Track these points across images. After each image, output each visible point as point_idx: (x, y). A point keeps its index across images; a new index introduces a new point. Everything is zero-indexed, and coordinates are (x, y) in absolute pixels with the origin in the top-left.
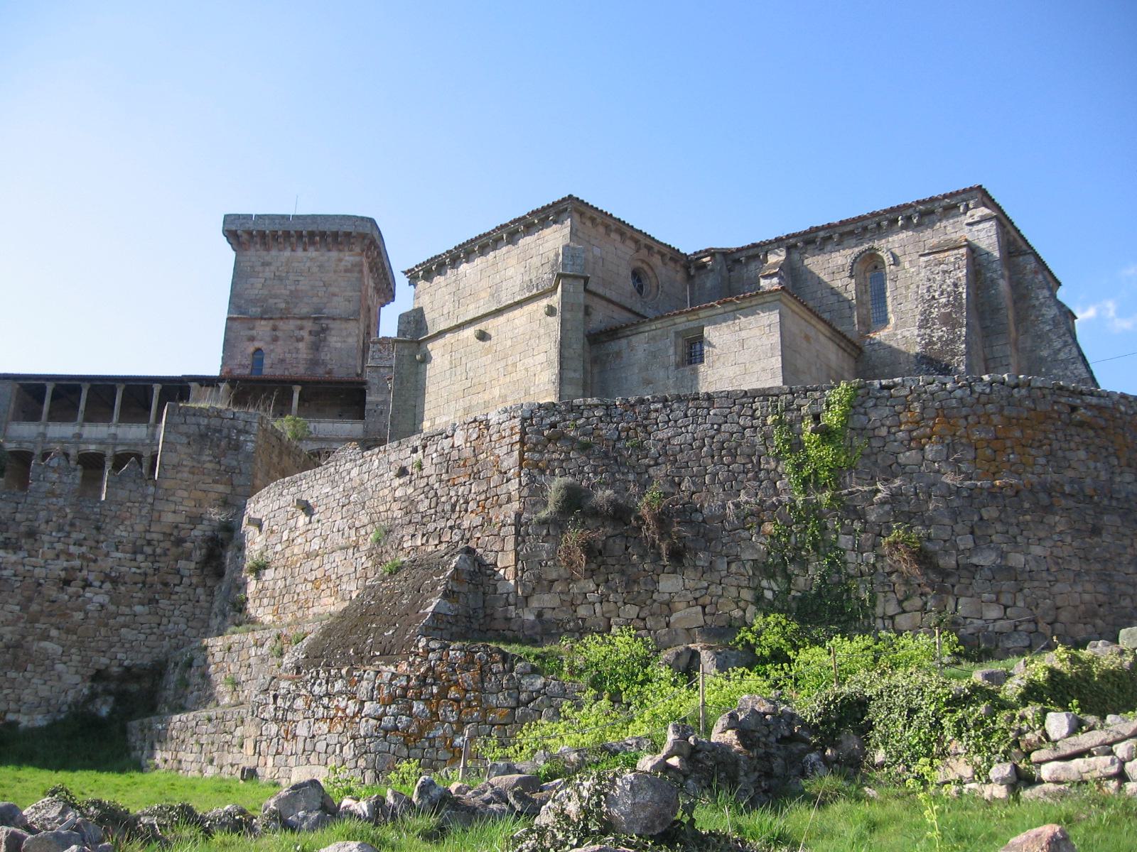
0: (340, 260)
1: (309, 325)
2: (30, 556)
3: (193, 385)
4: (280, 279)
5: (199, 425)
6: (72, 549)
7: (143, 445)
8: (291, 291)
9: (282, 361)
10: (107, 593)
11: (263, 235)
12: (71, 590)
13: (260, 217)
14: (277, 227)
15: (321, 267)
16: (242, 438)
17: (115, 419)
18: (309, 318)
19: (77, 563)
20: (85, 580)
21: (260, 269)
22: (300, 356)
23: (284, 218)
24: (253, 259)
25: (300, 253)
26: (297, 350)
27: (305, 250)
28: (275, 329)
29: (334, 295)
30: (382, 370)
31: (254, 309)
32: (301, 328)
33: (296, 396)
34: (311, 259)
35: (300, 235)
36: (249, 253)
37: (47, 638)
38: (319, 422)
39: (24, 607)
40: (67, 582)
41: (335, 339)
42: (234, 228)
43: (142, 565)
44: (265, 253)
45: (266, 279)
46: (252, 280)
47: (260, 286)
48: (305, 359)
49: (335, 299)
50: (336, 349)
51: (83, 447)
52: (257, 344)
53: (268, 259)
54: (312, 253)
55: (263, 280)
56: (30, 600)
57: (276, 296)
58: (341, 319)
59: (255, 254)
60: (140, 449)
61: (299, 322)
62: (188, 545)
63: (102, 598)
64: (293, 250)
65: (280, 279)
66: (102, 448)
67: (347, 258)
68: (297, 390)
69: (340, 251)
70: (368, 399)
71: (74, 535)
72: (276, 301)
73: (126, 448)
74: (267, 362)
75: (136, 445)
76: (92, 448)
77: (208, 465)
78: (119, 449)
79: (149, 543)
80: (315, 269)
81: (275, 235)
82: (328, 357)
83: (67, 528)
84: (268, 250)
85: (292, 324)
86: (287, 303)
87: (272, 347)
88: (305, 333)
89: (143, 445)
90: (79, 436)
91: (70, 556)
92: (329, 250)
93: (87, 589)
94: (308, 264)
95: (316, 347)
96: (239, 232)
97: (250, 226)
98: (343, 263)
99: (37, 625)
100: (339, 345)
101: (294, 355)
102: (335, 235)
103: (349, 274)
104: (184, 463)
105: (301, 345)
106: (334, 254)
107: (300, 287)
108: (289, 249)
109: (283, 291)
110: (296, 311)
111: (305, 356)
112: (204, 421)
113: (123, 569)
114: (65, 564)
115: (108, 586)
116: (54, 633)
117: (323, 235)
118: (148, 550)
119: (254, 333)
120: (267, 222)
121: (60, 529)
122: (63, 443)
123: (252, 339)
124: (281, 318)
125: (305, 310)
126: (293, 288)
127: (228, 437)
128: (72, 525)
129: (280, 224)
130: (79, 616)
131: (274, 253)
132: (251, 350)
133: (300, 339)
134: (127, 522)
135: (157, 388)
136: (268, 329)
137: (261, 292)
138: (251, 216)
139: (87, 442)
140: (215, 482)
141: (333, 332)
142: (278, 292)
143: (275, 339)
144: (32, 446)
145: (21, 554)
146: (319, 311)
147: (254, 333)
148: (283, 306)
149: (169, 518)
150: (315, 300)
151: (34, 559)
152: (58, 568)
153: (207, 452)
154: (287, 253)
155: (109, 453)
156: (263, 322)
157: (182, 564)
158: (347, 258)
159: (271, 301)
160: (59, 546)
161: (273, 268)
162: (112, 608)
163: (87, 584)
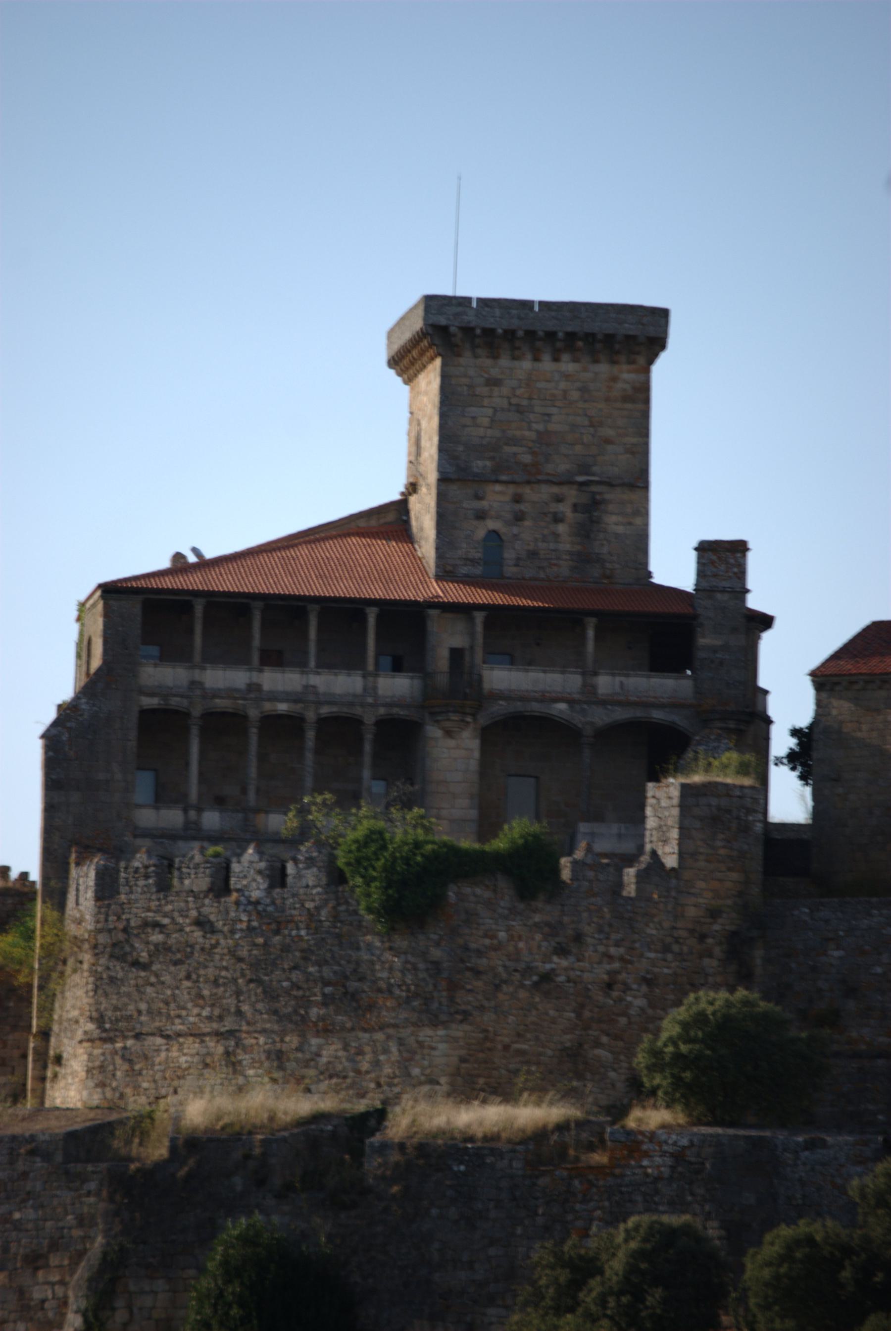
0: (614, 379)
1: (572, 494)
2: (579, 960)
3: (433, 612)
4: (519, 410)
5: (710, 805)
6: (613, 950)
7: (363, 705)
8: (538, 432)
9: (533, 554)
10: (645, 996)
11: (489, 333)
12: (615, 994)
13: (486, 303)
14: (515, 323)
15: (584, 390)
16: (751, 818)
17: (312, 663)
18: (570, 483)
19: (617, 965)
20: (625, 984)
21: (484, 390)
22: (561, 546)
23: (525, 305)
24: (471, 372)
25: (547, 365)
26: (556, 535)
27: (556, 359)
28: (518, 499)
29: (608, 441)
30: (719, 596)
31: (480, 463)
32: (559, 499)
33: (591, 633)
34: (567, 377)
35: (551, 336)
36: (462, 361)
37: (597, 1044)
38: (627, 676)
39: (579, 1016)
40: (609, 986)
41: (614, 519)
42: (443, 321)
43: (673, 965)
44: (489, 362)
45: (495, 410)
46: (473, 411)
47: (486, 421)
48: (569, 553)
49: (610, 448)
50: (617, 536)
51: (268, 706)
52: (491, 524)
53: (495, 372)
54: (567, 365)
55: (490, 412)
56: (582, 1006)
57: (514, 441)
58: (623, 485)
59: (473, 365)
60: (358, 711)
61: (555, 490)
62: (710, 941)
63: (640, 1002)
64: (536, 359)
65: (519, 410)
66: (298, 707)
67: (625, 376)
68: (372, 615)
69: (614, 362)
70: (702, 641)
71: (614, 936)
72: (515, 449)
73: (335, 709)
74: (509, 555)
75: (352, 704)
76: (282, 707)
77: (722, 852)
78: (325, 710)
79: (677, 940)
80: (575, 395)
81: (510, 335)
82: (605, 550)
83: (607, 929)
84: (495, 357)
85: (546, 492)
86: (534, 453)
87: (515, 530)
88: (565, 508)
89: (363, 705)
90: (254, 688)
91: (611, 958)
92: (596, 361)
93: (629, 993)
94: (563, 385)
95: (587, 529)
96: (453, 329)
97: (470, 318)
98: (620, 385)
99: (590, 1032)
100: (620, 529)
101: (552, 546)
102: (609, 339)
103: (629, 406)
104: (701, 850)
105: (561, 528)
106: (604, 368)
107: (552, 427)
108: (529, 356)
109: (527, 433)
110: (549, 468)
111: (568, 547)
112: (714, 801)
113: (656, 970)
114: (608, 967)
115: (644, 988)
116: (605, 1039)
117: (590, 338)
118: (676, 948)
119: (484, 504)
120: (497, 312)
121: (601, 931)
122: (236, 699)
123: (481, 516)
124: (528, 482)
125: (563, 466)
126: (540, 427)
127: (738, 818)
128: (610, 925)
129: (520, 318)
130: (623, 1021)
131: (505, 362)
132: (481, 533)
133: (558, 519)
134: (656, 920)
135: (372, 615)
136: (507, 498)
137: (489, 432)
138: (468, 300)
139: (274, 697)
140: (730, 869)
141: (611, 507)
142: (518, 433)
143: (519, 517)
144: (185, 702)
145: (572, 959)
146: (585, 469)
147: (484, 504)
148: (527, 459)
149: (691, 912)
150: (578, 449)
151: (581, 964)
152: (601, 972)
153: (721, 836)
154: (526, 364)
155: (311, 716)
156: (498, 488)
157: (707, 961)
158: (625, 376)
159: (508, 449)
160: (601, 949)
161: (505, 391)
162: (650, 1012)
163: (627, 988)
